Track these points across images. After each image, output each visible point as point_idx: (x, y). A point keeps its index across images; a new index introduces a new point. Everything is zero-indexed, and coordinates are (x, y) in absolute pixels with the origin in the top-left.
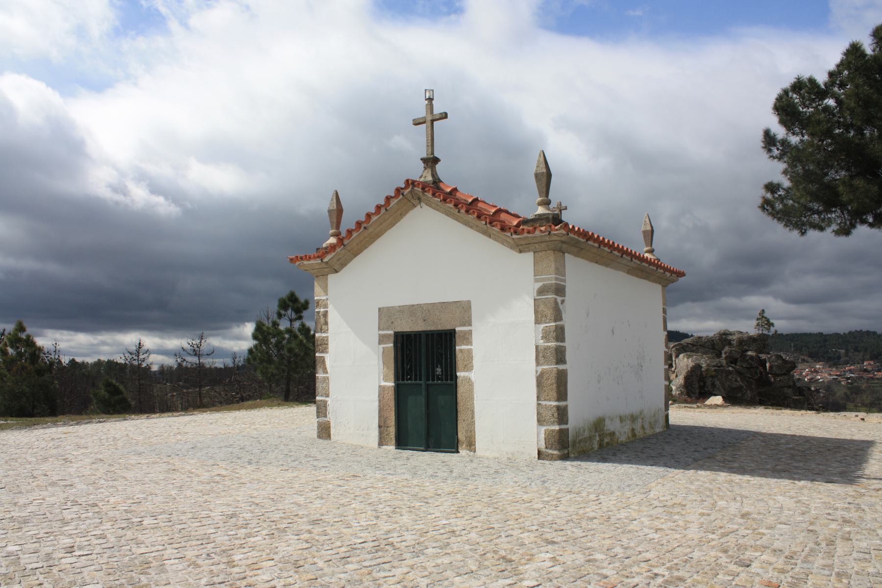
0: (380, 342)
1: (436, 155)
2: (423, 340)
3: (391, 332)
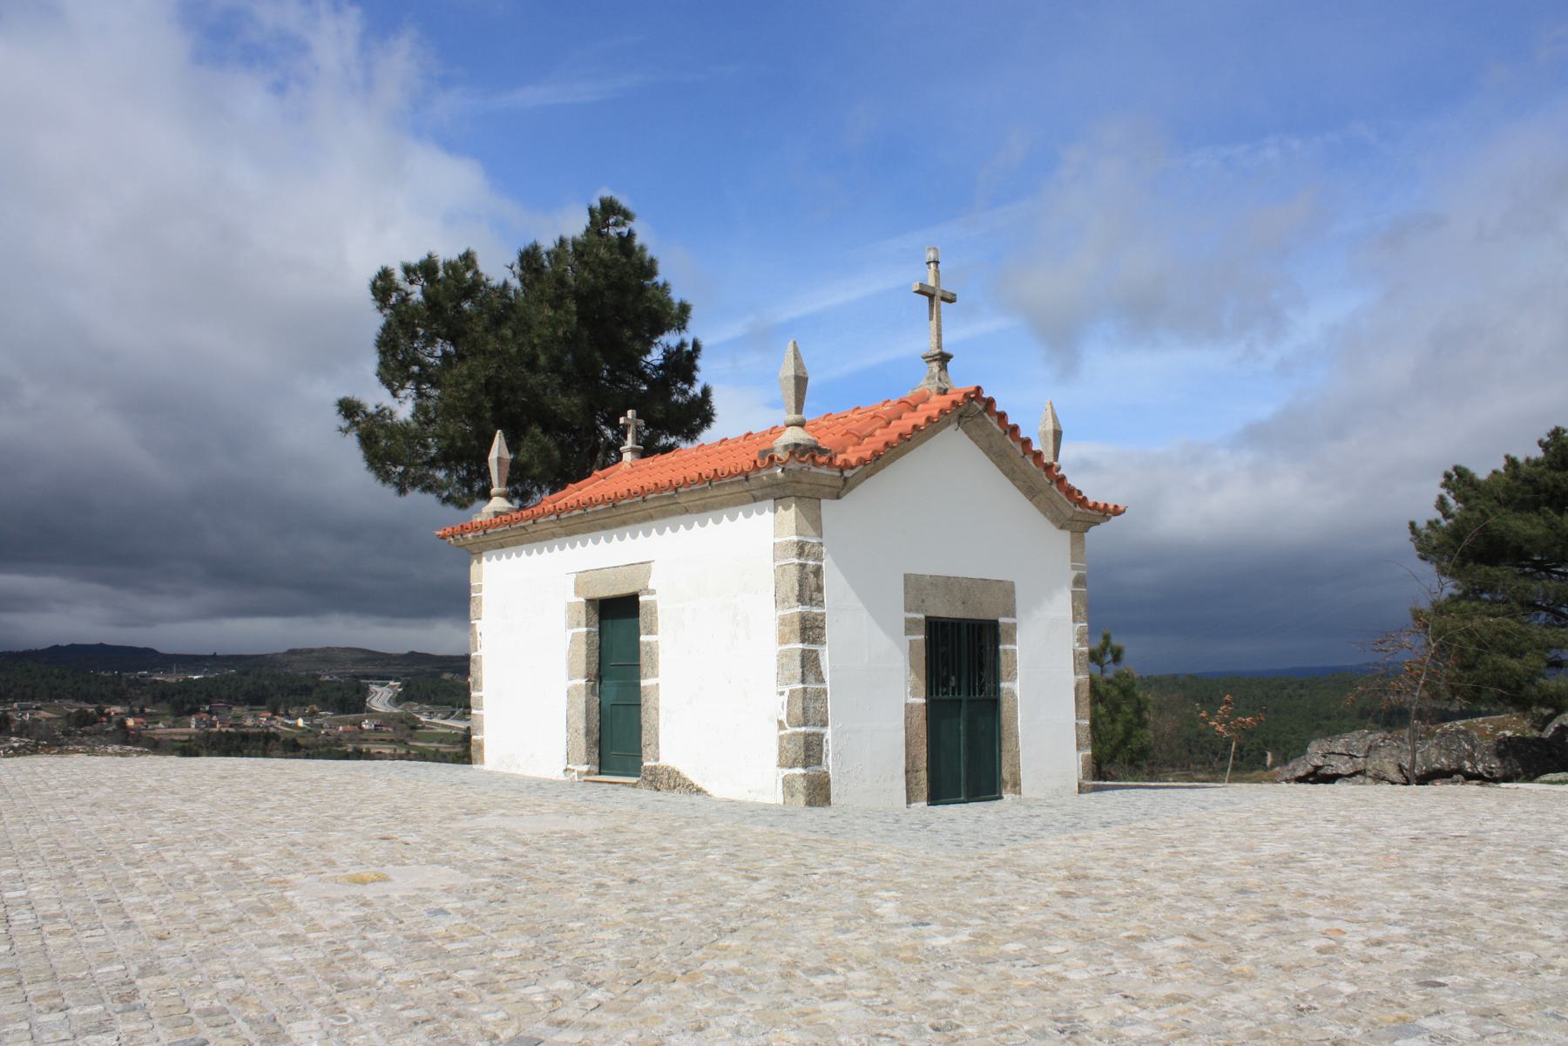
0: (908, 631)
1: (946, 350)
2: (964, 632)
3: (921, 616)
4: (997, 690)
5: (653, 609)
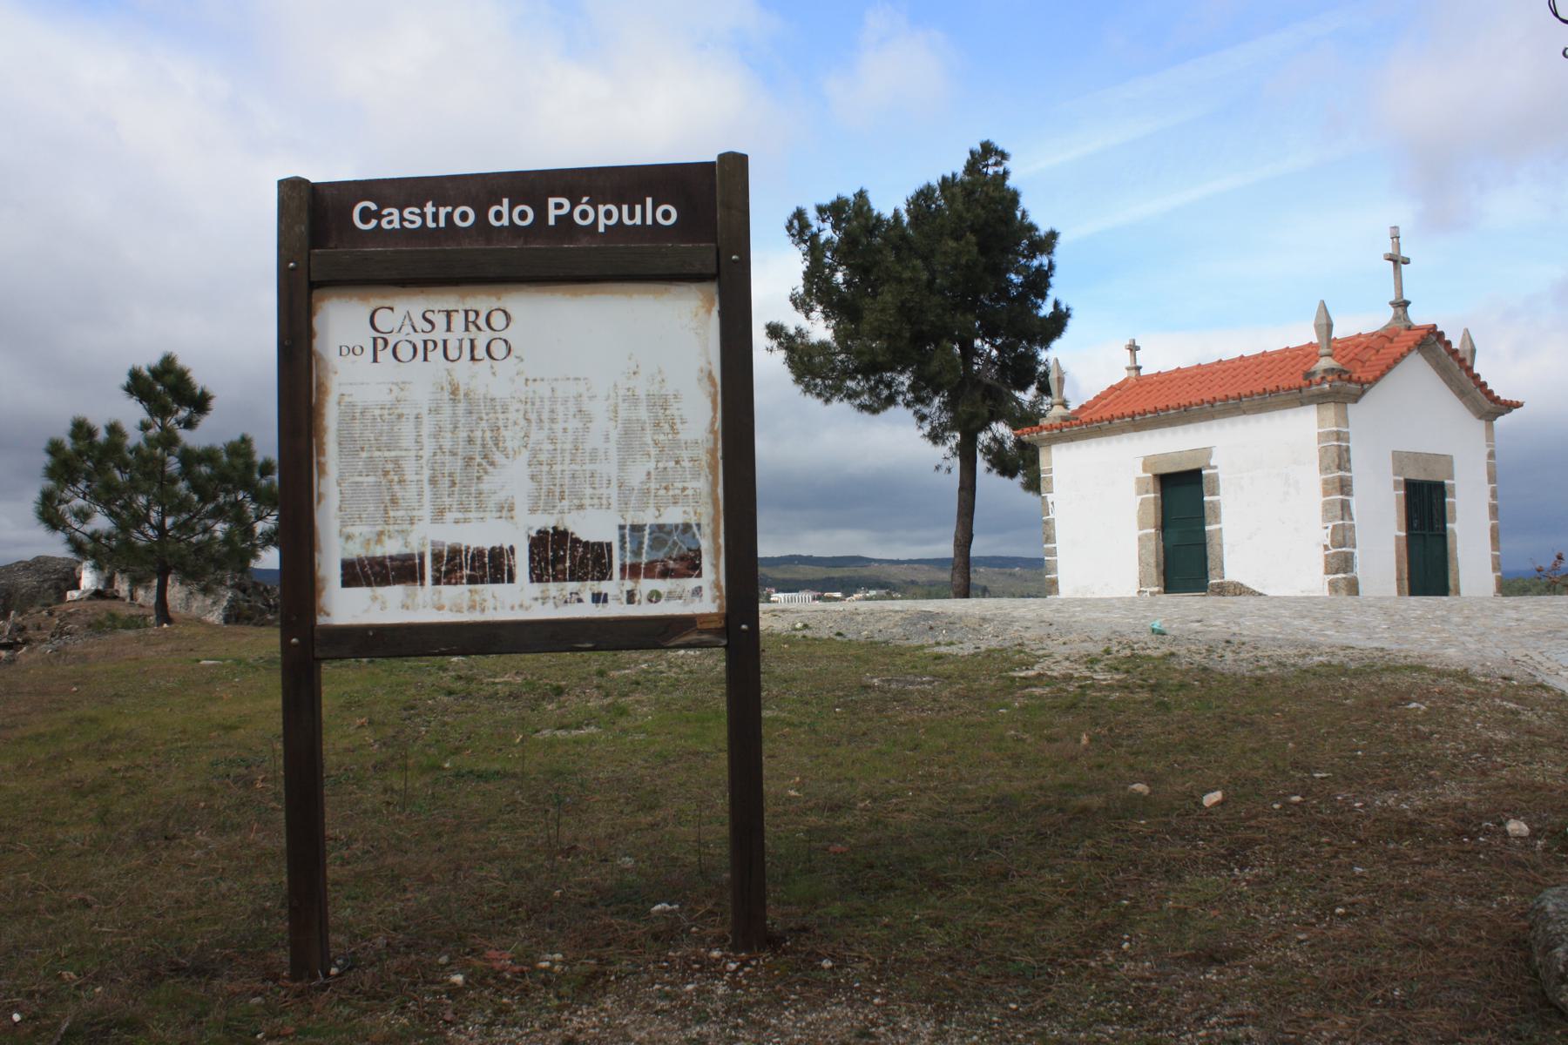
0: (1396, 488)
1: (1406, 297)
4: (1444, 529)
5: (1215, 479)
